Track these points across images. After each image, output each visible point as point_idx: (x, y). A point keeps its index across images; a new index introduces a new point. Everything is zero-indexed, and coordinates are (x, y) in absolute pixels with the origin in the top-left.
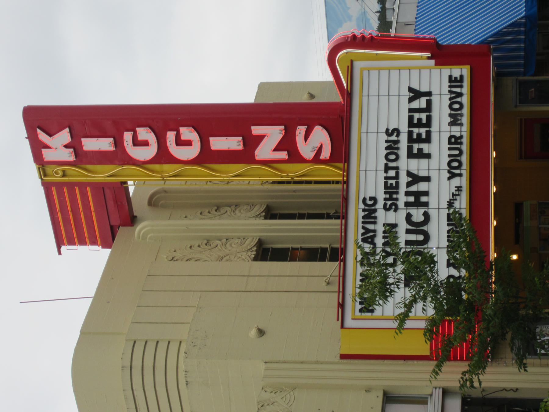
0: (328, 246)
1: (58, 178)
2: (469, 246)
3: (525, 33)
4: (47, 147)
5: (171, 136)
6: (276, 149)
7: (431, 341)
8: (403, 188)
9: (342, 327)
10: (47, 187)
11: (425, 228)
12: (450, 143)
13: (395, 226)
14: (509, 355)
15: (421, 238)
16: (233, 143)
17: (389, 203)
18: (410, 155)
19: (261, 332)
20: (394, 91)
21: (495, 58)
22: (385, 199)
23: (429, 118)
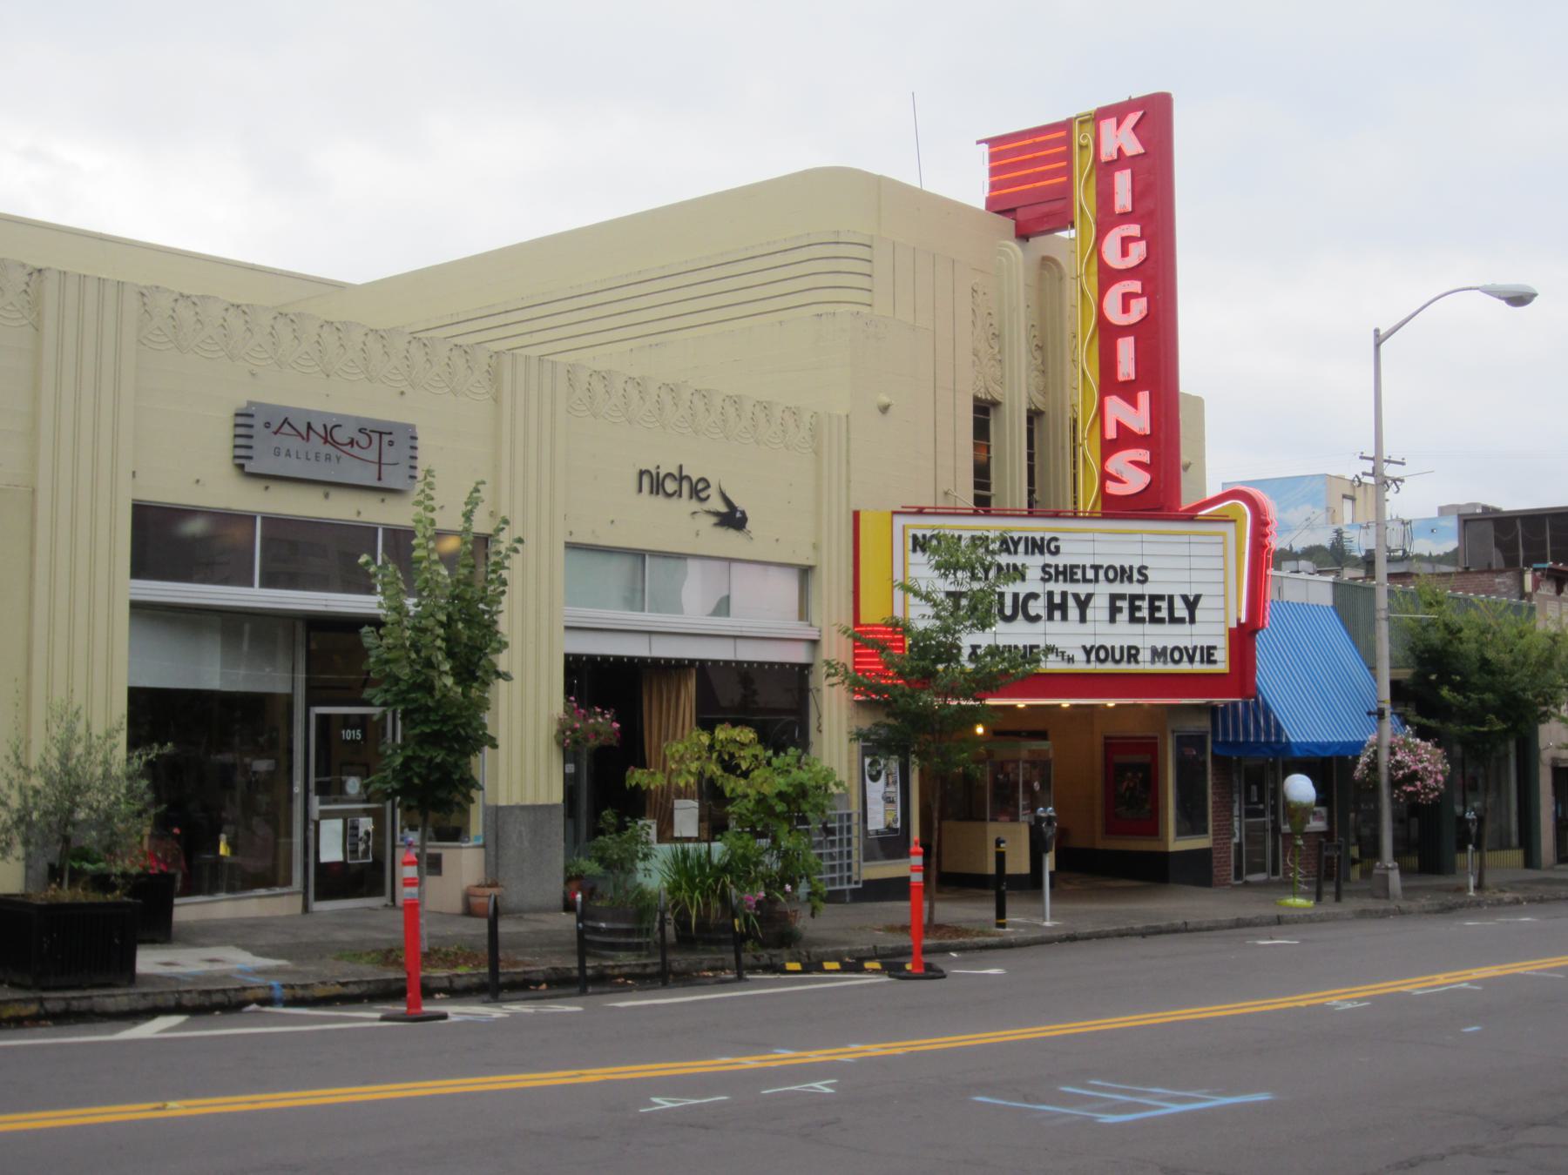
0: (993, 491)
1: (1077, 140)
2: (1004, 673)
3: (1268, 743)
4: (1119, 124)
5: (1135, 286)
6: (1119, 425)
7: (886, 625)
8: (1071, 588)
9: (894, 513)
10: (1066, 126)
11: (1020, 616)
12: (1130, 648)
13: (1023, 578)
14: (866, 722)
15: (1008, 611)
16: (1126, 368)
17: (1052, 571)
18: (1114, 598)
19: (884, 409)
20: (1196, 576)
21: (1235, 705)
22: (1057, 567)
23: (1161, 621)
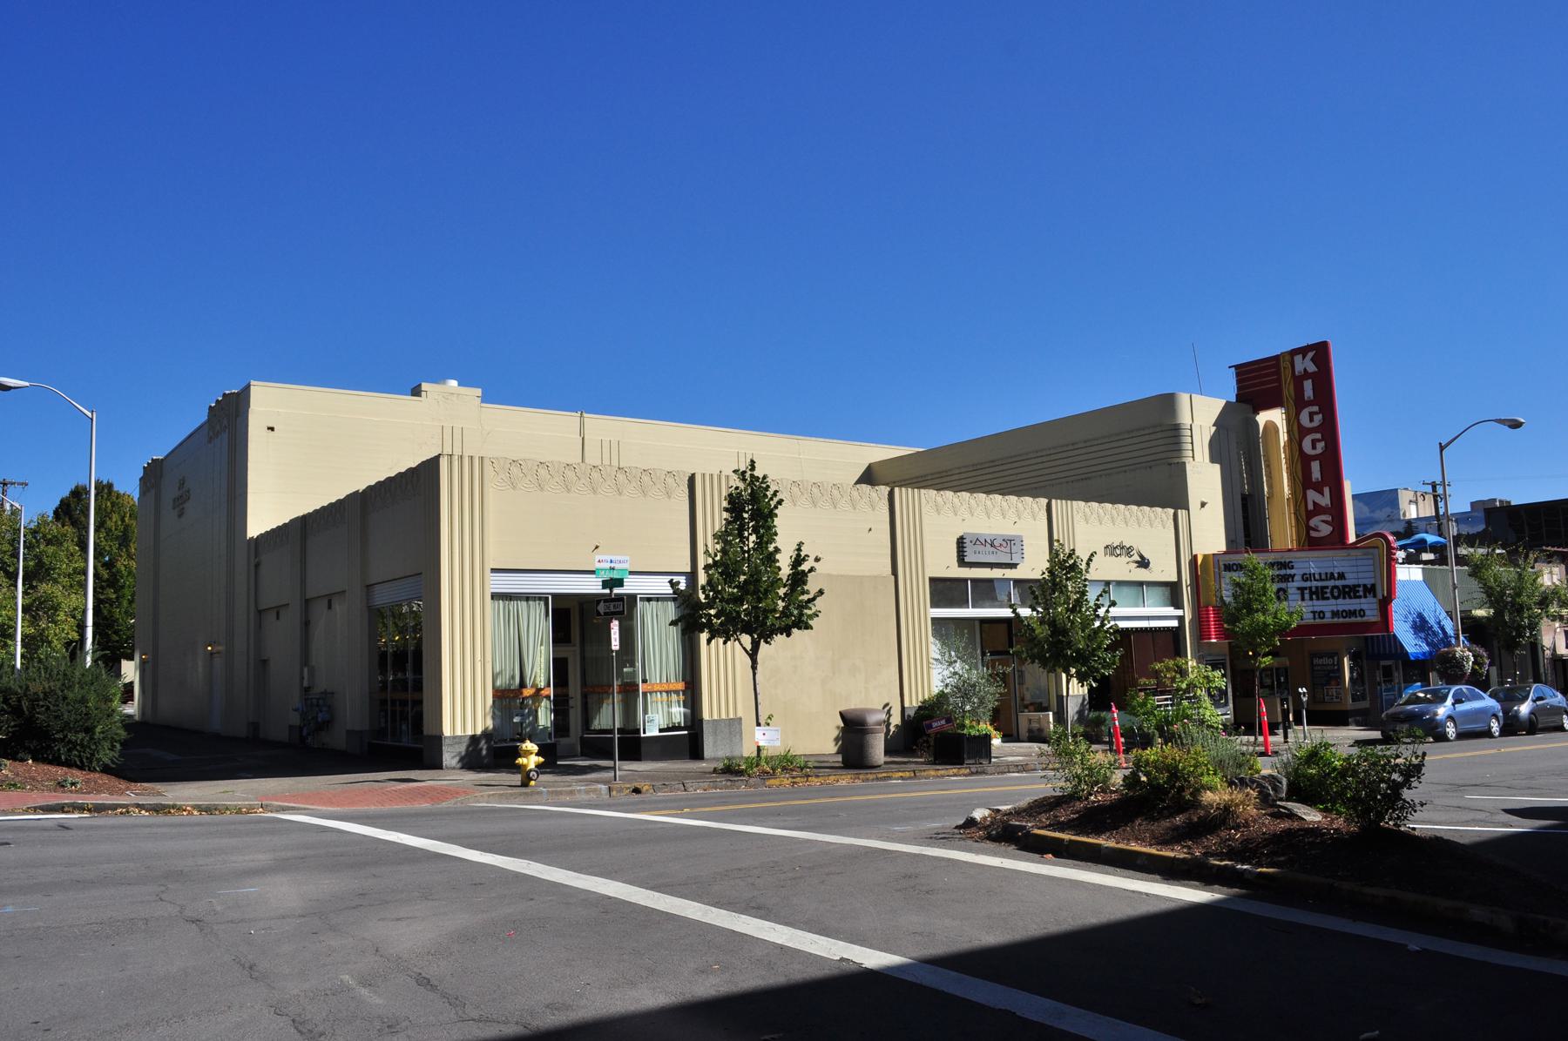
5: (1318, 436)
10: (1276, 358)
16: (1316, 473)
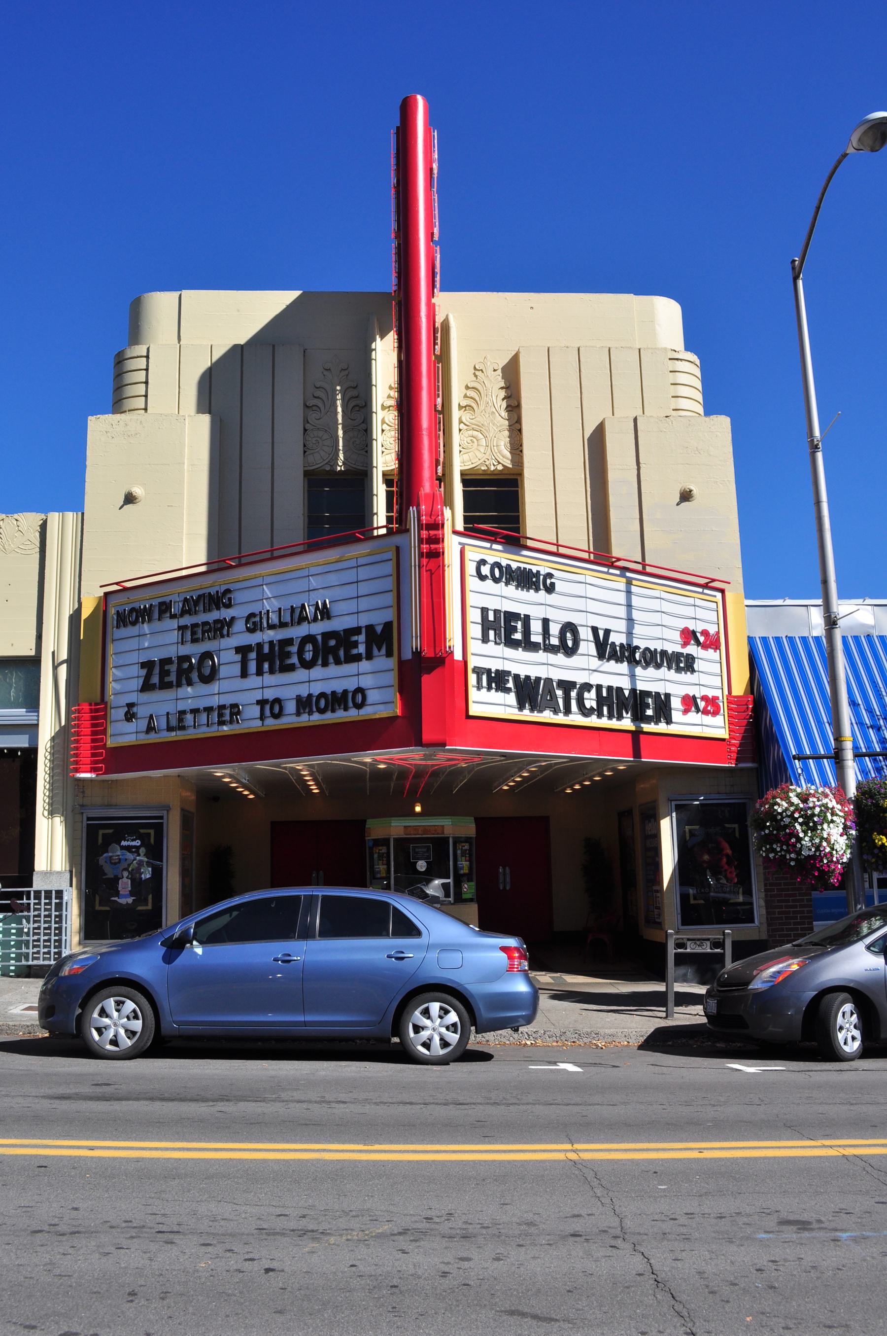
19: (130, 499)
